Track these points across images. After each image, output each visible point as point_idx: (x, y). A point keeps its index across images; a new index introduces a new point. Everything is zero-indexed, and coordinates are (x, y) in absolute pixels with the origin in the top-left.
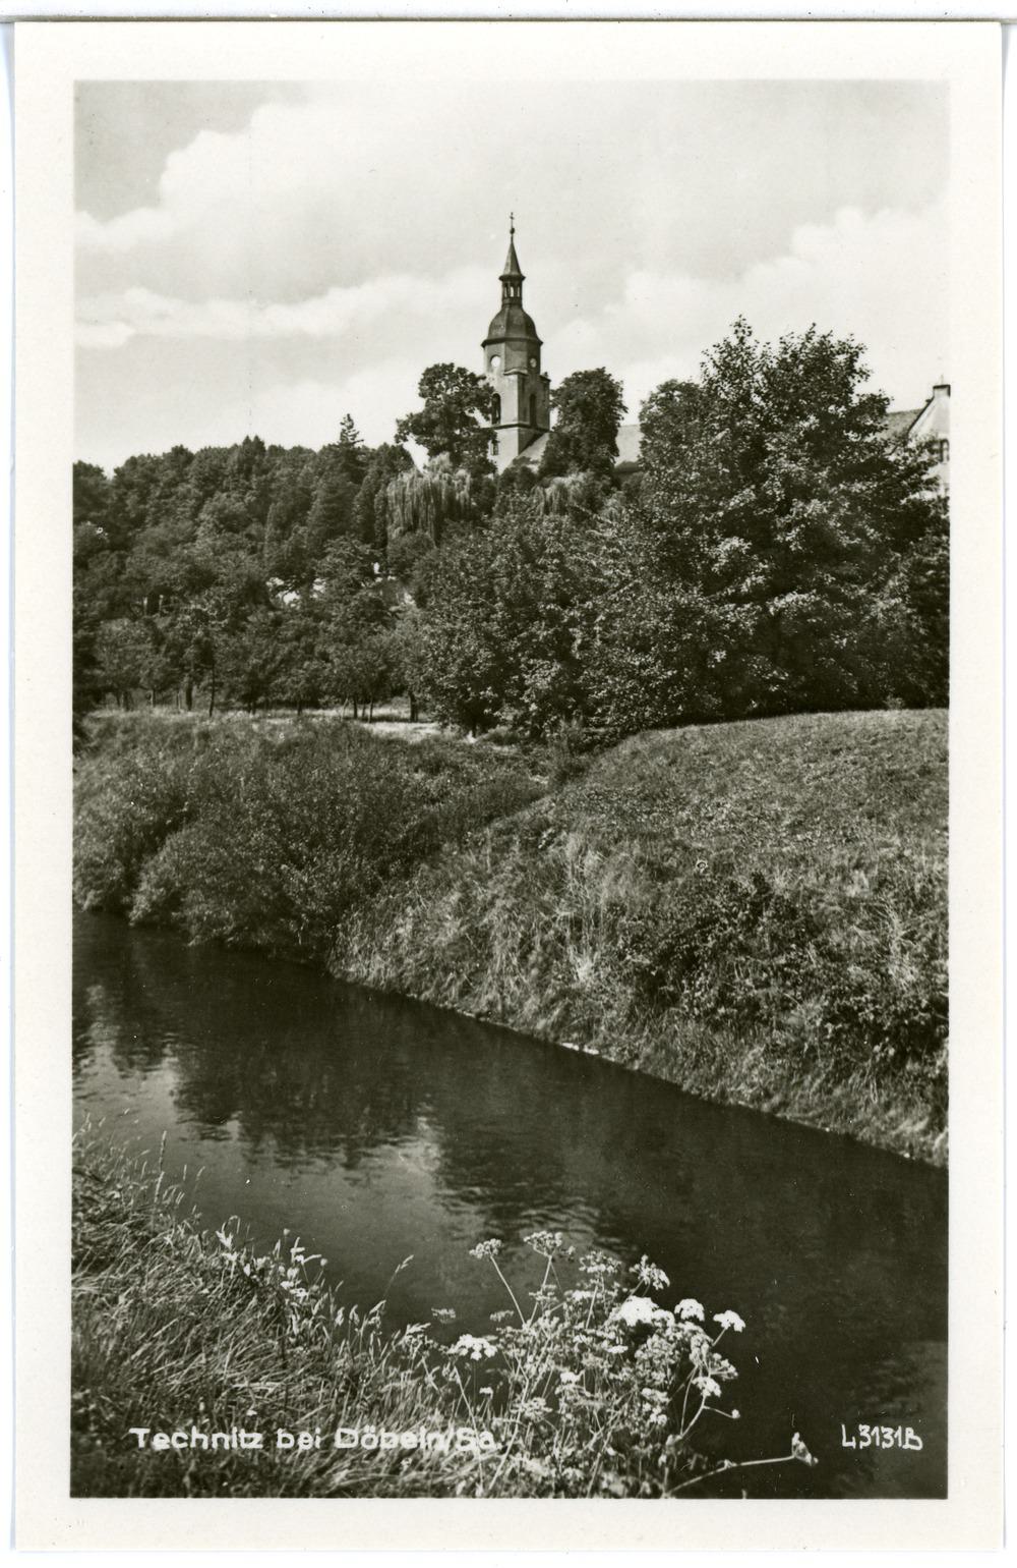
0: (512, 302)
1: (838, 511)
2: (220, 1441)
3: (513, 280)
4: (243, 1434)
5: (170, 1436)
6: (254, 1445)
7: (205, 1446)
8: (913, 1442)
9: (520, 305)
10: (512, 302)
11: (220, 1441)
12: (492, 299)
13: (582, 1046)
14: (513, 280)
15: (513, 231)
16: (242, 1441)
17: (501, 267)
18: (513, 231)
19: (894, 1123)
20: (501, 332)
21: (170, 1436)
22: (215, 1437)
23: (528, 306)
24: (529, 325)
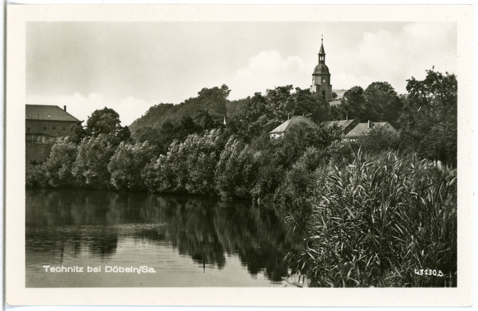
0: (322, 62)
1: (345, 179)
2: (70, 269)
3: (322, 54)
4: (77, 268)
5: (56, 268)
6: (80, 271)
7: (66, 271)
8: (441, 274)
9: (324, 63)
10: (322, 62)
11: (70, 269)
12: (315, 62)
13: (238, 166)
14: (322, 54)
15: (322, 40)
16: (77, 270)
17: (318, 51)
18: (322, 40)
19: (63, 164)
20: (320, 72)
21: (56, 268)
22: (69, 268)
23: (327, 63)
24: (327, 69)
